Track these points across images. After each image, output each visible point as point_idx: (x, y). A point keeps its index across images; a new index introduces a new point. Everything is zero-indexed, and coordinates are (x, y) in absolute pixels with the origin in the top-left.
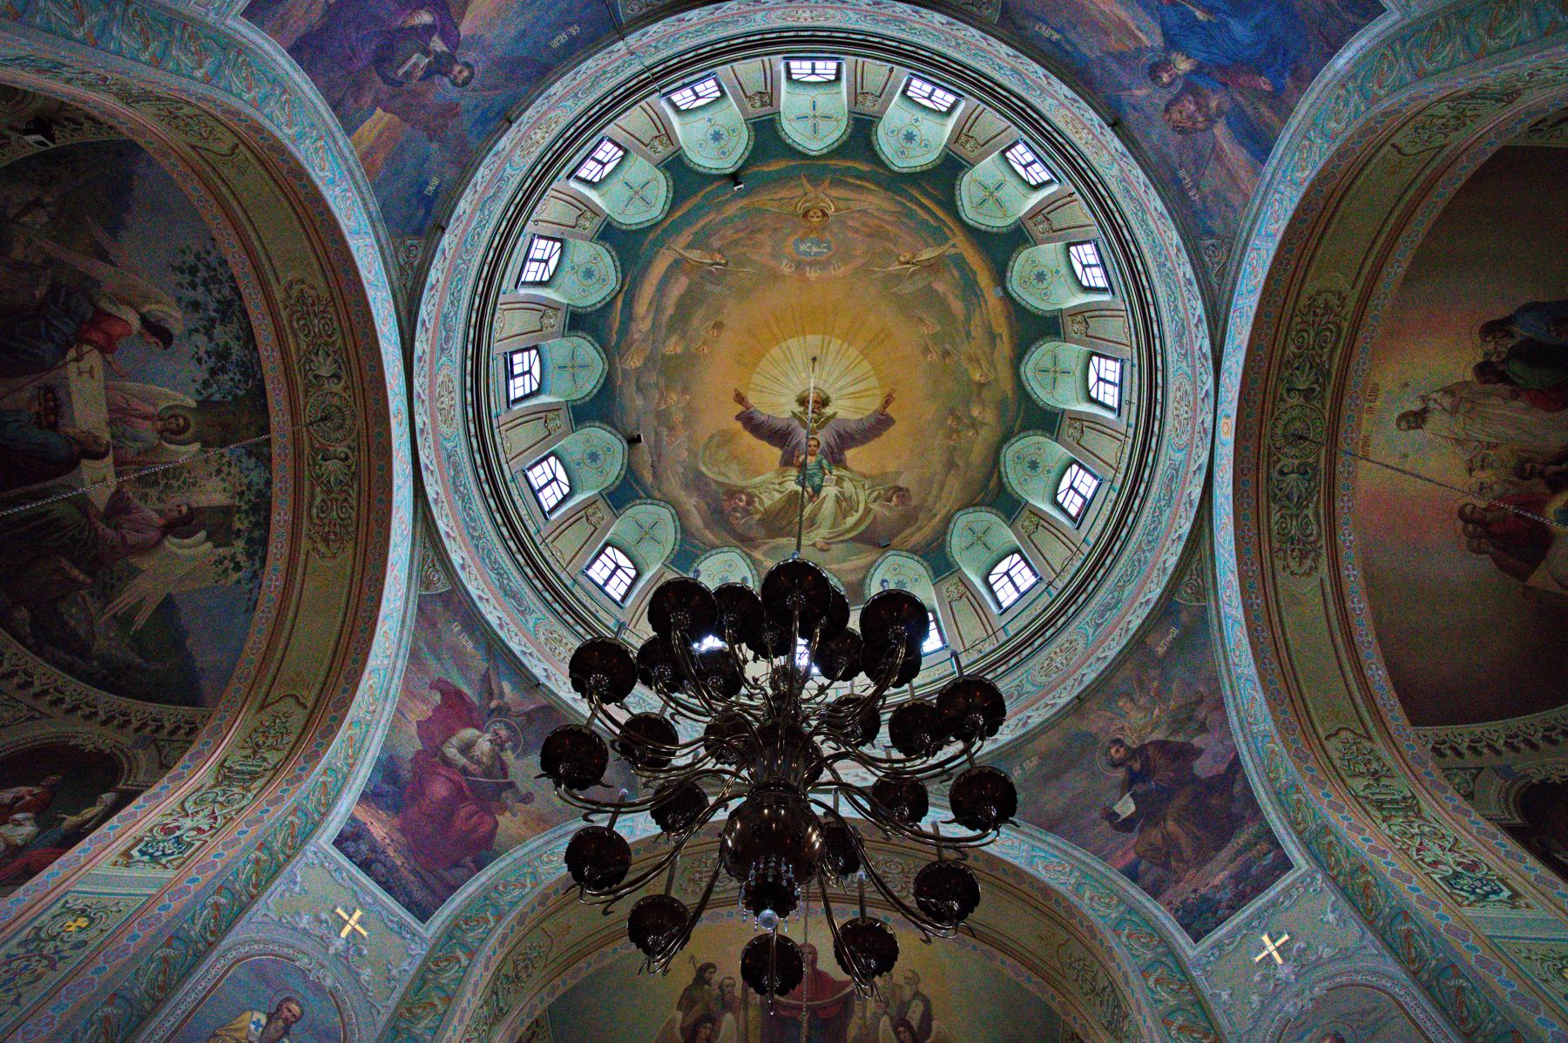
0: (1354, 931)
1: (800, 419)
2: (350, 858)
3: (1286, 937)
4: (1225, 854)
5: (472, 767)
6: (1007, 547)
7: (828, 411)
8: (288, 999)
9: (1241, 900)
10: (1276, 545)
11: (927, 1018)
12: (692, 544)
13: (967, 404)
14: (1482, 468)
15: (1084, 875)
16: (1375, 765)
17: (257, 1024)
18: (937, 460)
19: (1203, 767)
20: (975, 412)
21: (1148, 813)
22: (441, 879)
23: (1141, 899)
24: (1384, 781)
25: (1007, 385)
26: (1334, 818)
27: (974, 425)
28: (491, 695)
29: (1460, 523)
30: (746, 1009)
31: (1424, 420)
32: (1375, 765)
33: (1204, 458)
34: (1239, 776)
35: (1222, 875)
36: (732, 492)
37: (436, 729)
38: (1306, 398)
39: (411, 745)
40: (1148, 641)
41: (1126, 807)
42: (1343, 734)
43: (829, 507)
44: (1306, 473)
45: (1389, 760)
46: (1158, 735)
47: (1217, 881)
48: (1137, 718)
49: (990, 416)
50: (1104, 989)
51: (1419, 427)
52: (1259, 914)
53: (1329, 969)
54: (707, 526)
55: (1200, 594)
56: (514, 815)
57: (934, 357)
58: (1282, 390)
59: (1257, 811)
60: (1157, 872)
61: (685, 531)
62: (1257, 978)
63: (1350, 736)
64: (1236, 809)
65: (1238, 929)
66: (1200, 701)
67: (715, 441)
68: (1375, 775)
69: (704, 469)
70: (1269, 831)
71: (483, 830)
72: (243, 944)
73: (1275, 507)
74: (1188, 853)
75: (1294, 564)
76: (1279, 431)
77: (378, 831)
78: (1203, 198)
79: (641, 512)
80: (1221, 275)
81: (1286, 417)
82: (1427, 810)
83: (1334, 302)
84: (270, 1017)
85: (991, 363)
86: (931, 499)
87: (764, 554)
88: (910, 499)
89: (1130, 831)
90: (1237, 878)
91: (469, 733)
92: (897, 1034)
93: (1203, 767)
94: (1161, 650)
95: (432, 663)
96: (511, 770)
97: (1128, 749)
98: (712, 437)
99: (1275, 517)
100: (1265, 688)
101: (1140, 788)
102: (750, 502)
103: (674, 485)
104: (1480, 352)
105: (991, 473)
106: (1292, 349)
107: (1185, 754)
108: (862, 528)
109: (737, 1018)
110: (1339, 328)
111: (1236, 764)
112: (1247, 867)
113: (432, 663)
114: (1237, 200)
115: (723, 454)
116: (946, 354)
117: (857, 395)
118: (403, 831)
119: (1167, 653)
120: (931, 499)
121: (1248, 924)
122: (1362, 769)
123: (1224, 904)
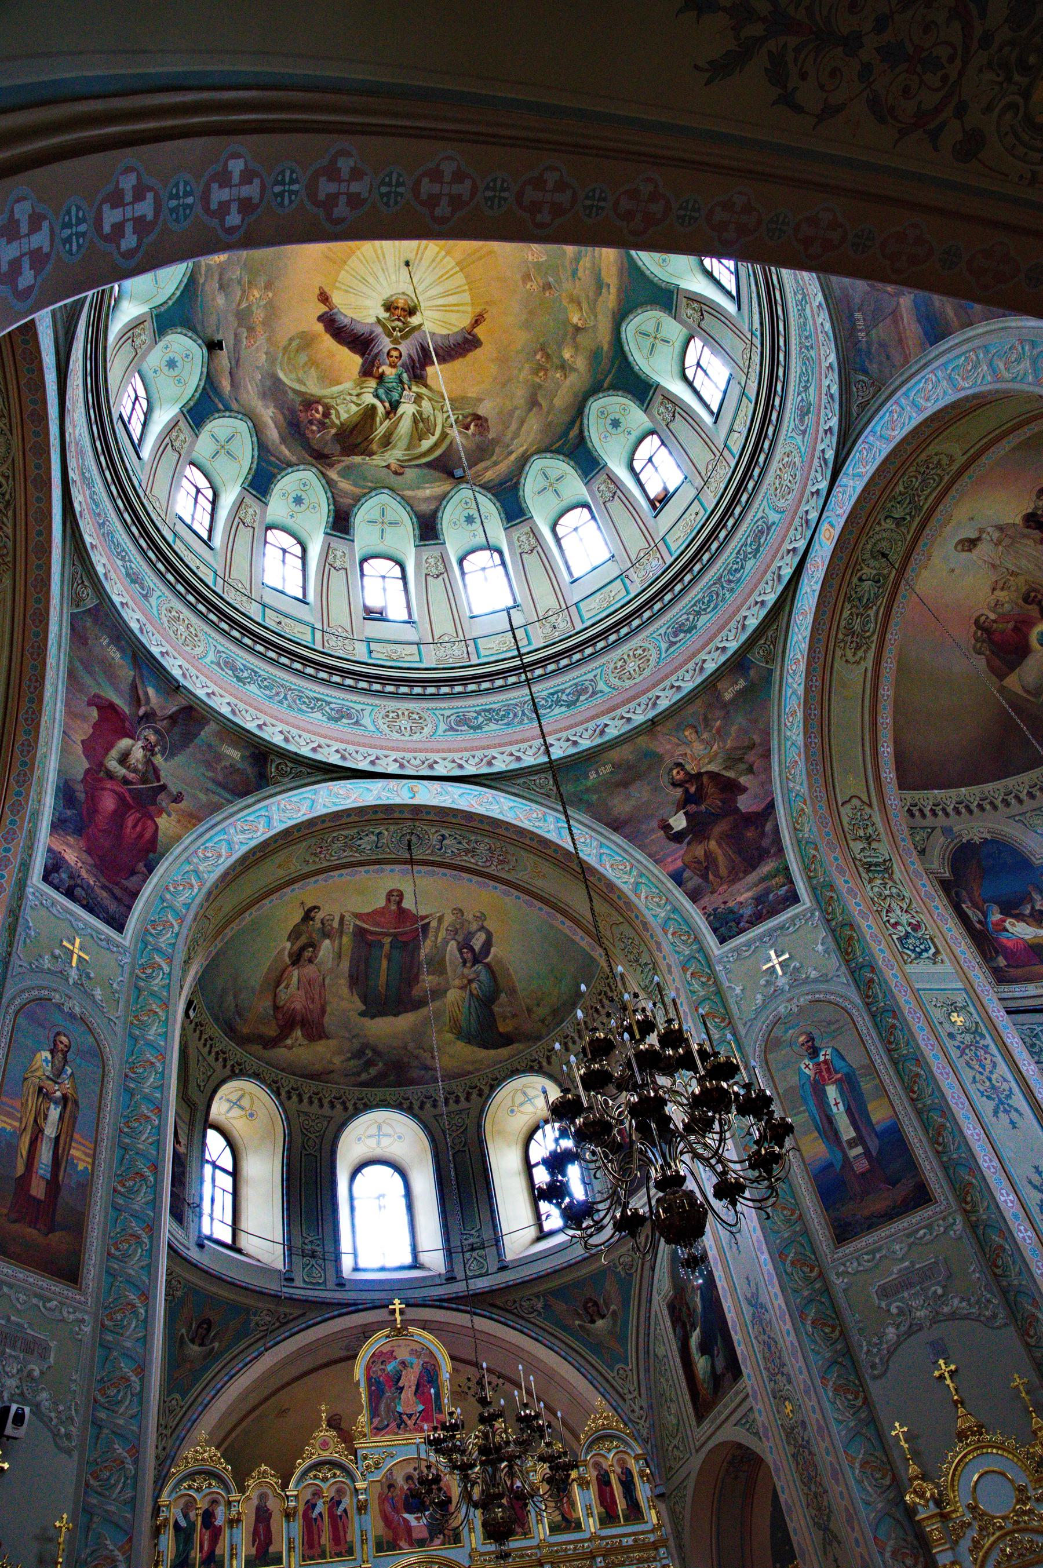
0: (834, 962)
1: (384, 326)
2: (57, 889)
3: (787, 956)
4: (753, 877)
5: (131, 776)
6: (574, 500)
7: (415, 321)
8: (58, 1034)
9: (758, 918)
10: (840, 636)
11: (488, 944)
12: (270, 464)
13: (560, 345)
14: (1002, 589)
15: (641, 875)
16: (870, 830)
17: (46, 1060)
18: (520, 395)
19: (745, 803)
20: (567, 354)
21: (697, 829)
22: (125, 889)
23: (683, 901)
24: (874, 845)
25: (604, 336)
26: (839, 881)
27: (563, 367)
28: (139, 706)
29: (974, 628)
30: (341, 937)
31: (975, 545)
32: (870, 830)
33: (801, 545)
34: (771, 817)
35: (749, 894)
36: (310, 403)
37: (96, 747)
38: (898, 525)
39: (81, 765)
40: (719, 686)
41: (679, 822)
42: (855, 801)
43: (405, 426)
44: (878, 581)
45: (881, 829)
46: (713, 767)
47: (741, 899)
48: (698, 748)
49: (581, 363)
50: (646, 964)
51: (970, 550)
52: (770, 933)
53: (813, 987)
54: (283, 440)
55: (770, 658)
56: (169, 815)
57: (533, 286)
58: (881, 517)
59: (781, 850)
60: (695, 879)
61: (262, 447)
62: (762, 982)
63: (859, 803)
64: (766, 842)
65: (753, 941)
66: (752, 746)
67: (295, 344)
68: (869, 839)
69: (281, 375)
70: (787, 868)
71: (148, 835)
72: (14, 998)
73: (848, 606)
74: (723, 871)
75: (849, 653)
76: (869, 547)
77: (71, 857)
78: (869, 343)
79: (220, 426)
80: (863, 407)
81: (877, 537)
82: (897, 876)
83: (945, 461)
84: (52, 1052)
85: (593, 310)
86: (509, 434)
87: (339, 473)
88: (488, 429)
89: (680, 842)
90: (758, 900)
91: (125, 743)
92: (461, 953)
93: (745, 803)
94: (728, 696)
95: (88, 680)
96: (163, 774)
97: (687, 773)
98: (291, 339)
99: (846, 614)
100: (807, 758)
101: (692, 808)
102: (326, 414)
103: (251, 395)
104: (1032, 506)
105: (573, 422)
106: (900, 488)
107: (731, 788)
108: (438, 453)
109: (333, 944)
110: (941, 478)
111: (771, 806)
112: (767, 892)
113: (88, 680)
114: (897, 358)
115: (303, 358)
116: (548, 286)
117: (445, 308)
118: (89, 852)
119: (732, 701)
120: (509, 434)
121: (760, 938)
122: (861, 833)
123: (745, 919)
